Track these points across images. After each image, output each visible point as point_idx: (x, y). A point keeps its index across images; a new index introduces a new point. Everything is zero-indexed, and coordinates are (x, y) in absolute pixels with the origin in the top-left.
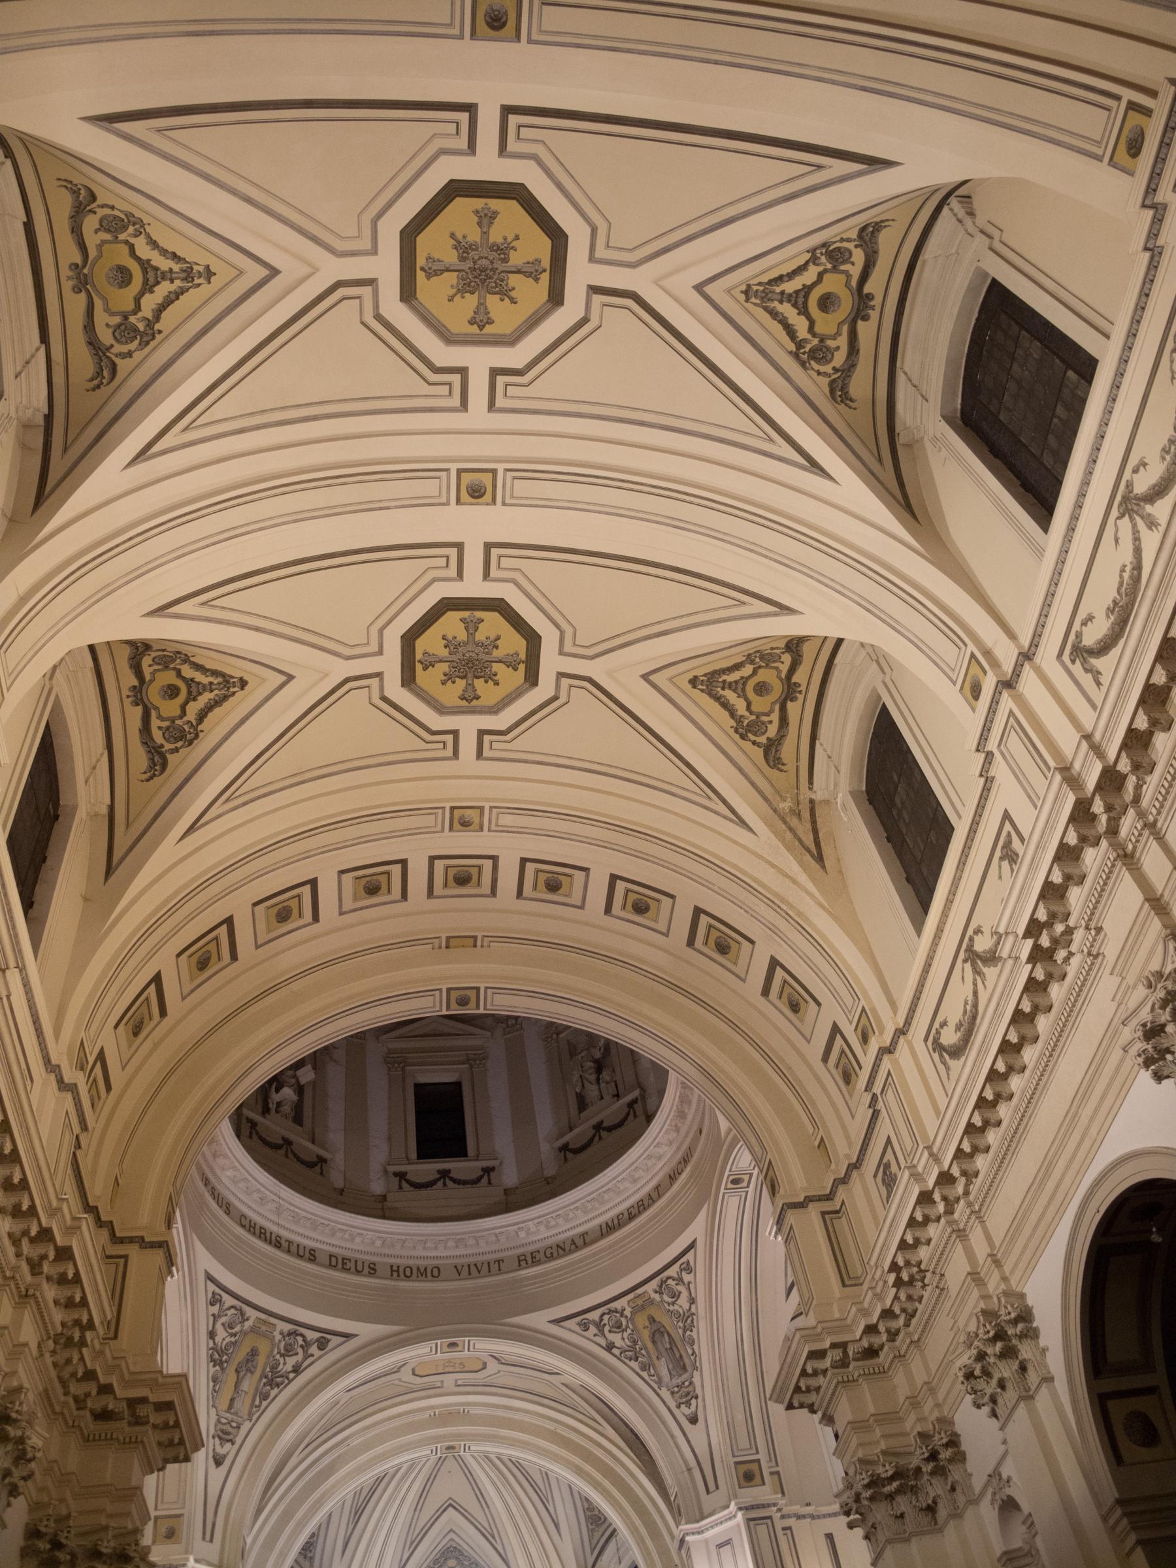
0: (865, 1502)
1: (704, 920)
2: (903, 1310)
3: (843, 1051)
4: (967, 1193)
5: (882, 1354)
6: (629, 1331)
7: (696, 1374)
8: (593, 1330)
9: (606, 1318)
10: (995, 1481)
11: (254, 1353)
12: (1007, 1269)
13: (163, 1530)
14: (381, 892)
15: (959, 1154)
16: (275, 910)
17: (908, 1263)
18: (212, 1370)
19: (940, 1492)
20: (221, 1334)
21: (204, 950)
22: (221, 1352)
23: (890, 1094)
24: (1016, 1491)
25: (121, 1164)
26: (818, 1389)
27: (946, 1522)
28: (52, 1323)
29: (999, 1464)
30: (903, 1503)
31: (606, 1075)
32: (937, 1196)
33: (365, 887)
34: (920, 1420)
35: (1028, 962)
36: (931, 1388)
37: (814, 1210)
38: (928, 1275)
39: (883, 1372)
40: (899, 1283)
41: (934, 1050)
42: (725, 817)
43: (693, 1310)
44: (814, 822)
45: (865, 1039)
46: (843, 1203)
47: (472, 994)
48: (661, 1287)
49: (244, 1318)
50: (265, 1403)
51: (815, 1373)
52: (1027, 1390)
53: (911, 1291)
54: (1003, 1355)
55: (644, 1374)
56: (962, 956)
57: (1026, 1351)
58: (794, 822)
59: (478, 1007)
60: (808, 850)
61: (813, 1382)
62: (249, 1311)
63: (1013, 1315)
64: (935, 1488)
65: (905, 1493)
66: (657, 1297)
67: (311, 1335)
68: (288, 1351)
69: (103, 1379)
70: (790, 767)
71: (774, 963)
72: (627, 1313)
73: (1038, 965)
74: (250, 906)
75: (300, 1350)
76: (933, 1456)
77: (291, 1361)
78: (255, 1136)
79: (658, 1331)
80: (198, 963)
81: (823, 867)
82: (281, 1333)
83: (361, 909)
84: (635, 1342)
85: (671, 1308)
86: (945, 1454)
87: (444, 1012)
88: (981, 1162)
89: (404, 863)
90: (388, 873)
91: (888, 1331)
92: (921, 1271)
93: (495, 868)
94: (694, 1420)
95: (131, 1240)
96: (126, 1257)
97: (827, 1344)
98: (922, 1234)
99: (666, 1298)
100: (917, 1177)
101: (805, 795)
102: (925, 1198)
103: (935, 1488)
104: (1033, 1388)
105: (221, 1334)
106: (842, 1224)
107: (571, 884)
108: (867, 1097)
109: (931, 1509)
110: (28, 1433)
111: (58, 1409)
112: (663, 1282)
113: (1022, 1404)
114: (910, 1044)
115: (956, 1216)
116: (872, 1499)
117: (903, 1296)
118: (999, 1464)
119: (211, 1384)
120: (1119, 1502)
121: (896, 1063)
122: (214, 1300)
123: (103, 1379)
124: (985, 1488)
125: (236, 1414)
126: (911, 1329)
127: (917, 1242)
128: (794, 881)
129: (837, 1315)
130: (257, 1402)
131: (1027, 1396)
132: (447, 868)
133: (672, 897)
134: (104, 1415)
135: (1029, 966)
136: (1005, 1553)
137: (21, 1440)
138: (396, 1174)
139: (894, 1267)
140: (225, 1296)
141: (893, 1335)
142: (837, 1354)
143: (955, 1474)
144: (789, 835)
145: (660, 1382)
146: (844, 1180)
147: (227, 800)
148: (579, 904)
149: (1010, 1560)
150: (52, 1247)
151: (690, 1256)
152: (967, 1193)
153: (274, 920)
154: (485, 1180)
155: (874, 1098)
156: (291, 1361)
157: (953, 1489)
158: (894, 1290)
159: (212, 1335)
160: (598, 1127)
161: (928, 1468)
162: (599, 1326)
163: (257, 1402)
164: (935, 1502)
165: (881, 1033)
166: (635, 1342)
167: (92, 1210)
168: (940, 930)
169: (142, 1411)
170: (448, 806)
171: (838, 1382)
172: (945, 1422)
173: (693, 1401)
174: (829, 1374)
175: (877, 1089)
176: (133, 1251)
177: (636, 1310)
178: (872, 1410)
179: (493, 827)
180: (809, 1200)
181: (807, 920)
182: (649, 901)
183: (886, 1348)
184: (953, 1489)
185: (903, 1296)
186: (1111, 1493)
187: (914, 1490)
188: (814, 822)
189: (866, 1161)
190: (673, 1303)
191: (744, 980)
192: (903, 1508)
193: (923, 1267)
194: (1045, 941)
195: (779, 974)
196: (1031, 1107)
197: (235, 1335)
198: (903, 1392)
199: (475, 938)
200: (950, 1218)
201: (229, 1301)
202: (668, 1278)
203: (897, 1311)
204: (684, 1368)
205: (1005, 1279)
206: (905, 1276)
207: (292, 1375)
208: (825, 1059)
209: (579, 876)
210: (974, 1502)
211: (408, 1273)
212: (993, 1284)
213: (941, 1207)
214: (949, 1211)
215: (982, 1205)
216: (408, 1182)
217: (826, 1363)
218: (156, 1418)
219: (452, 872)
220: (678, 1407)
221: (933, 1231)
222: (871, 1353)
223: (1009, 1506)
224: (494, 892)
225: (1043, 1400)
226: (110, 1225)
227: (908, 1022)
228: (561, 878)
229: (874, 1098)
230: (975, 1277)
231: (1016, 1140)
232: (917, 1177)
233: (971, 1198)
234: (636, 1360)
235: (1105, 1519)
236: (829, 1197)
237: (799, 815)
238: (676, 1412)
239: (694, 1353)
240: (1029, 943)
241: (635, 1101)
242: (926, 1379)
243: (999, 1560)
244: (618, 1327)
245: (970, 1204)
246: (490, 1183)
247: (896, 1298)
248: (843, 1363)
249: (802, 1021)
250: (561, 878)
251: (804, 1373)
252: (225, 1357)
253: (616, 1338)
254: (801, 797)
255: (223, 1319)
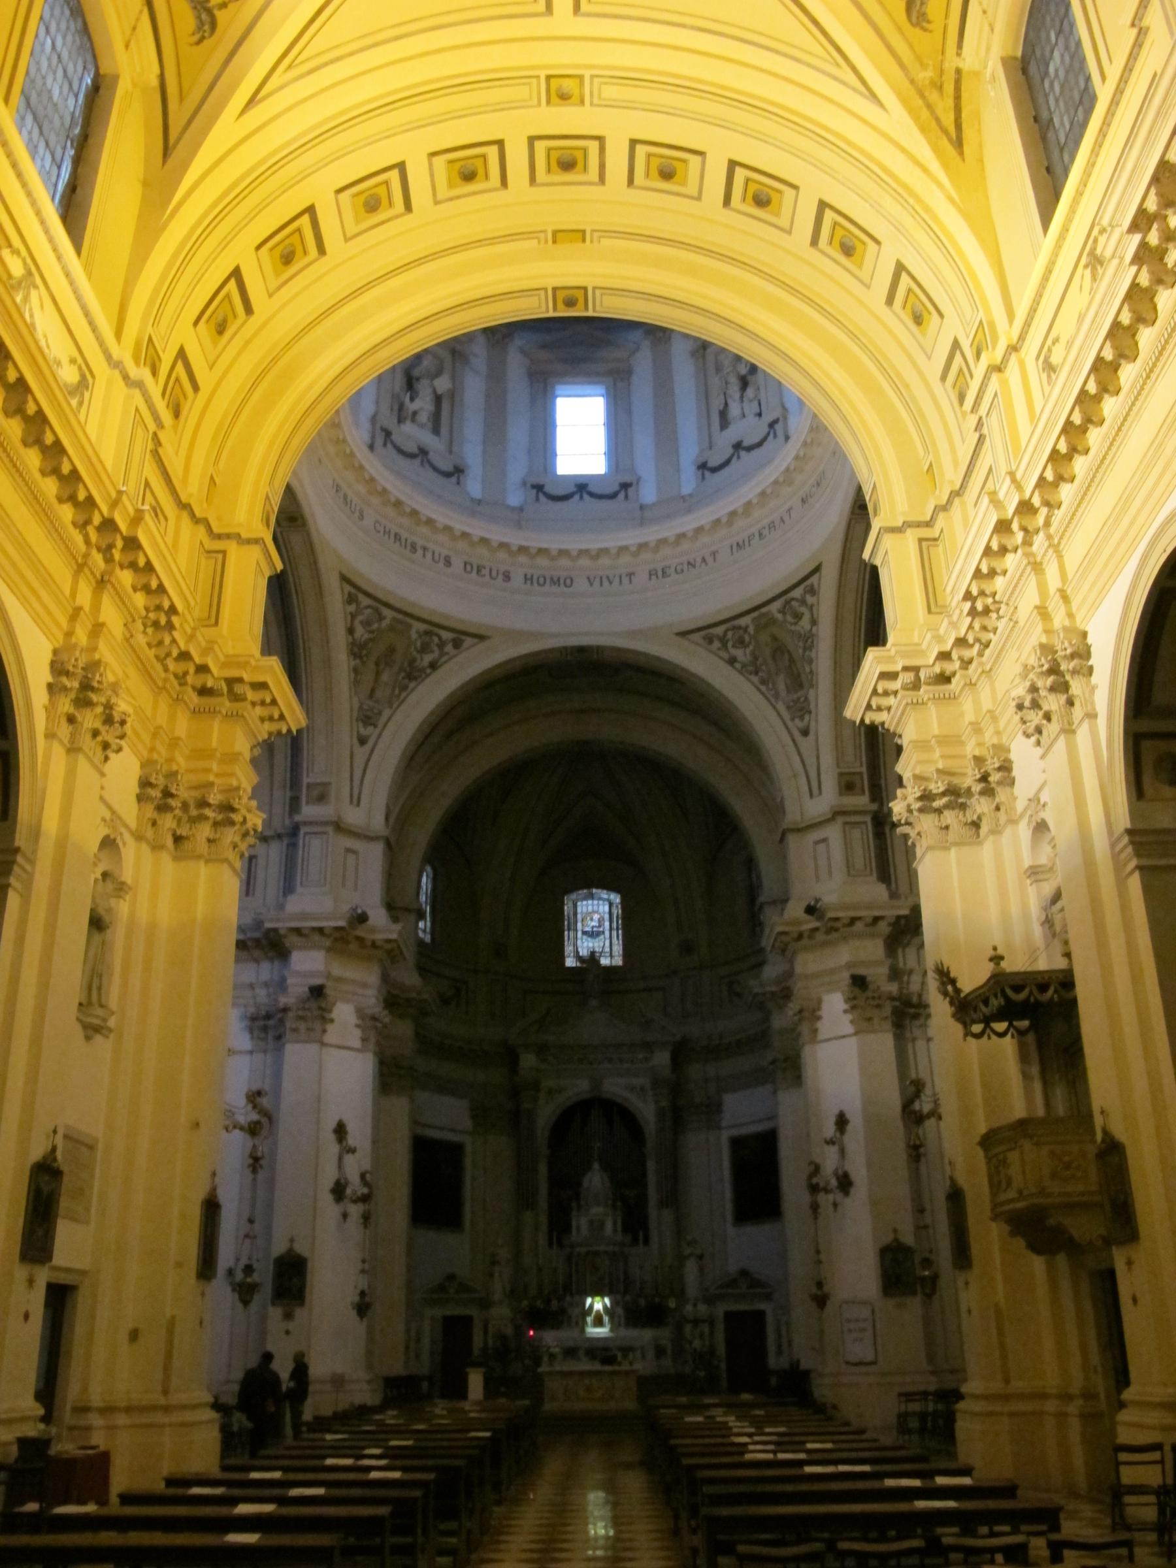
0: (915, 813)
1: (829, 215)
2: (977, 640)
3: (961, 370)
4: (1047, 524)
5: (954, 681)
6: (751, 647)
7: (812, 692)
8: (717, 644)
9: (730, 634)
10: (1033, 804)
11: (391, 650)
12: (1074, 605)
13: (315, 793)
14: (477, 178)
15: (1041, 481)
16: (362, 198)
17: (982, 593)
18: (353, 663)
19: (986, 810)
20: (360, 631)
21: (287, 242)
22: (363, 646)
23: (994, 415)
24: (1048, 816)
25: (216, 462)
26: (889, 709)
27: (987, 836)
28: (136, 609)
29: (1040, 789)
30: (949, 817)
31: (750, 392)
32: (1015, 526)
33: (460, 173)
34: (980, 744)
35: (1133, 262)
36: (993, 716)
37: (911, 536)
38: (1003, 606)
39: (954, 698)
40: (973, 612)
41: (1044, 370)
42: (854, 90)
43: (814, 629)
44: (958, 97)
45: (978, 355)
46: (942, 531)
47: (579, 295)
48: (784, 607)
49: (381, 618)
50: (404, 694)
51: (886, 693)
52: (1070, 723)
53: (986, 622)
54: (1052, 689)
55: (763, 688)
56: (1083, 261)
57: (1076, 686)
58: (933, 96)
59: (586, 308)
60: (945, 131)
61: (885, 702)
62: (386, 612)
63: (1069, 651)
64: (981, 806)
65: (953, 809)
66: (779, 616)
67: (446, 635)
68: (425, 649)
69: (198, 660)
70: (937, 26)
71: (900, 268)
72: (751, 630)
73: (1145, 268)
74: (333, 194)
75: (436, 648)
76: (984, 778)
77: (428, 658)
78: (389, 445)
79: (779, 650)
80: (282, 256)
81: (961, 153)
82: (417, 632)
83: (458, 197)
84: (756, 658)
85: (793, 628)
86: (994, 778)
87: (551, 314)
88: (1066, 492)
89: (500, 143)
90: (484, 157)
91: (961, 659)
92: (995, 602)
93: (602, 150)
94: (805, 733)
95: (228, 536)
96: (224, 553)
97: (898, 667)
98: (998, 565)
99: (789, 618)
100: (996, 502)
101: (951, 62)
102: (1003, 527)
103: (981, 806)
104: (1076, 722)
105: (360, 631)
106: (938, 552)
107: (686, 170)
108: (973, 420)
109: (976, 825)
110: (113, 700)
111: (160, 684)
112: (787, 603)
113: (1062, 737)
114: (1022, 364)
115: (1035, 548)
116: (921, 810)
117: (977, 625)
118: (1040, 789)
119: (353, 675)
120: (1129, 832)
121: (1004, 383)
122: (351, 599)
123: (198, 660)
124: (1025, 810)
125: (377, 701)
126: (984, 659)
127: (992, 573)
128: (925, 170)
129: (916, 640)
130: (397, 692)
131: (1069, 731)
132: (549, 150)
133: (795, 187)
134: (204, 691)
135: (1134, 269)
136: (1031, 867)
137: (109, 706)
138: (533, 487)
139: (968, 596)
140: (361, 597)
141: (966, 663)
142: (908, 677)
143: (1002, 795)
144: (925, 114)
145: (777, 696)
146: (945, 508)
147: (289, 67)
148: (696, 194)
149: (1034, 873)
150: (118, 537)
151: (814, 580)
152: (1047, 524)
153: (362, 210)
154: (622, 495)
155: (979, 424)
156: (428, 658)
157: (998, 808)
158: (969, 619)
159: (351, 631)
160: (738, 446)
161: (977, 788)
162: (723, 641)
163: (397, 692)
164: (979, 818)
165: (994, 348)
166: (756, 658)
167: (185, 506)
168: (1065, 229)
169: (238, 689)
170: (543, 74)
171: (907, 704)
172: (1001, 749)
173: (807, 717)
174: (899, 696)
175: (983, 410)
176: (232, 547)
177: (760, 628)
178: (936, 732)
179: (596, 101)
180: (907, 525)
181: (935, 217)
182: (772, 193)
183: (958, 676)
184: (998, 808)
185: (977, 625)
186: (1123, 820)
187: (963, 807)
188: (958, 97)
189: (968, 489)
190: (796, 624)
191: (868, 287)
192: (949, 821)
193: (997, 598)
194: (1153, 238)
195: (905, 280)
196: (1122, 434)
197: (372, 632)
198: (969, 717)
199: (584, 232)
200: (1027, 549)
201: (365, 601)
202: (793, 599)
203: (971, 641)
204: (801, 686)
205: (1070, 615)
206: (979, 606)
207: (428, 671)
208: (944, 378)
209: (695, 160)
210: (1013, 822)
211: (542, 580)
212: (1059, 619)
213: (1019, 536)
214: (1027, 543)
215: (1061, 538)
216: (546, 494)
217: (896, 685)
218: (251, 695)
219: (555, 155)
220: (793, 719)
221: (1011, 561)
222: (945, 679)
223: (1041, 827)
224: (602, 179)
225: (1083, 734)
226: (205, 522)
227: (1022, 337)
228: (675, 163)
229: (979, 424)
230: (1043, 612)
231: (1101, 471)
232: (996, 502)
233: (1052, 530)
234: (756, 673)
235: (1113, 846)
236: (928, 524)
237: (940, 88)
238: (790, 723)
239: (811, 672)
240: (1137, 238)
241: (776, 421)
242: (990, 707)
243: (1026, 872)
244: (741, 643)
245: (1049, 537)
246: (626, 497)
247: (970, 627)
248: (916, 685)
249: (924, 334)
250: (675, 163)
251: (875, 692)
252: (364, 652)
253: (739, 653)
254: (946, 65)
255: (360, 618)
